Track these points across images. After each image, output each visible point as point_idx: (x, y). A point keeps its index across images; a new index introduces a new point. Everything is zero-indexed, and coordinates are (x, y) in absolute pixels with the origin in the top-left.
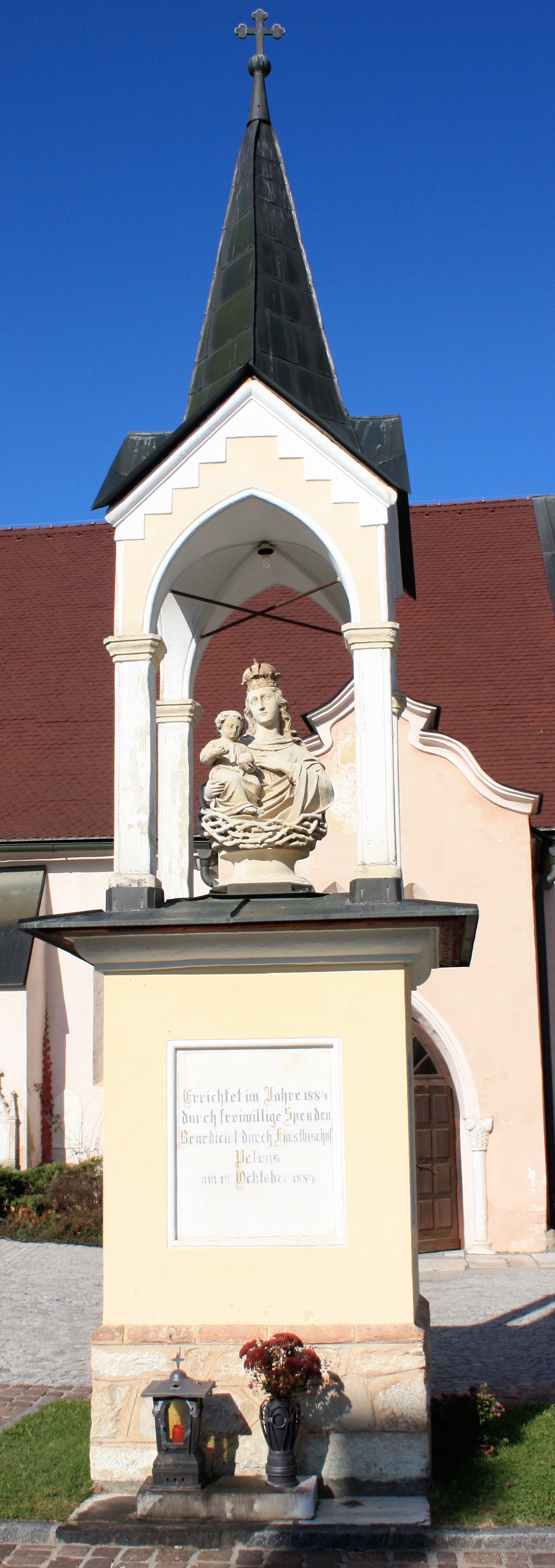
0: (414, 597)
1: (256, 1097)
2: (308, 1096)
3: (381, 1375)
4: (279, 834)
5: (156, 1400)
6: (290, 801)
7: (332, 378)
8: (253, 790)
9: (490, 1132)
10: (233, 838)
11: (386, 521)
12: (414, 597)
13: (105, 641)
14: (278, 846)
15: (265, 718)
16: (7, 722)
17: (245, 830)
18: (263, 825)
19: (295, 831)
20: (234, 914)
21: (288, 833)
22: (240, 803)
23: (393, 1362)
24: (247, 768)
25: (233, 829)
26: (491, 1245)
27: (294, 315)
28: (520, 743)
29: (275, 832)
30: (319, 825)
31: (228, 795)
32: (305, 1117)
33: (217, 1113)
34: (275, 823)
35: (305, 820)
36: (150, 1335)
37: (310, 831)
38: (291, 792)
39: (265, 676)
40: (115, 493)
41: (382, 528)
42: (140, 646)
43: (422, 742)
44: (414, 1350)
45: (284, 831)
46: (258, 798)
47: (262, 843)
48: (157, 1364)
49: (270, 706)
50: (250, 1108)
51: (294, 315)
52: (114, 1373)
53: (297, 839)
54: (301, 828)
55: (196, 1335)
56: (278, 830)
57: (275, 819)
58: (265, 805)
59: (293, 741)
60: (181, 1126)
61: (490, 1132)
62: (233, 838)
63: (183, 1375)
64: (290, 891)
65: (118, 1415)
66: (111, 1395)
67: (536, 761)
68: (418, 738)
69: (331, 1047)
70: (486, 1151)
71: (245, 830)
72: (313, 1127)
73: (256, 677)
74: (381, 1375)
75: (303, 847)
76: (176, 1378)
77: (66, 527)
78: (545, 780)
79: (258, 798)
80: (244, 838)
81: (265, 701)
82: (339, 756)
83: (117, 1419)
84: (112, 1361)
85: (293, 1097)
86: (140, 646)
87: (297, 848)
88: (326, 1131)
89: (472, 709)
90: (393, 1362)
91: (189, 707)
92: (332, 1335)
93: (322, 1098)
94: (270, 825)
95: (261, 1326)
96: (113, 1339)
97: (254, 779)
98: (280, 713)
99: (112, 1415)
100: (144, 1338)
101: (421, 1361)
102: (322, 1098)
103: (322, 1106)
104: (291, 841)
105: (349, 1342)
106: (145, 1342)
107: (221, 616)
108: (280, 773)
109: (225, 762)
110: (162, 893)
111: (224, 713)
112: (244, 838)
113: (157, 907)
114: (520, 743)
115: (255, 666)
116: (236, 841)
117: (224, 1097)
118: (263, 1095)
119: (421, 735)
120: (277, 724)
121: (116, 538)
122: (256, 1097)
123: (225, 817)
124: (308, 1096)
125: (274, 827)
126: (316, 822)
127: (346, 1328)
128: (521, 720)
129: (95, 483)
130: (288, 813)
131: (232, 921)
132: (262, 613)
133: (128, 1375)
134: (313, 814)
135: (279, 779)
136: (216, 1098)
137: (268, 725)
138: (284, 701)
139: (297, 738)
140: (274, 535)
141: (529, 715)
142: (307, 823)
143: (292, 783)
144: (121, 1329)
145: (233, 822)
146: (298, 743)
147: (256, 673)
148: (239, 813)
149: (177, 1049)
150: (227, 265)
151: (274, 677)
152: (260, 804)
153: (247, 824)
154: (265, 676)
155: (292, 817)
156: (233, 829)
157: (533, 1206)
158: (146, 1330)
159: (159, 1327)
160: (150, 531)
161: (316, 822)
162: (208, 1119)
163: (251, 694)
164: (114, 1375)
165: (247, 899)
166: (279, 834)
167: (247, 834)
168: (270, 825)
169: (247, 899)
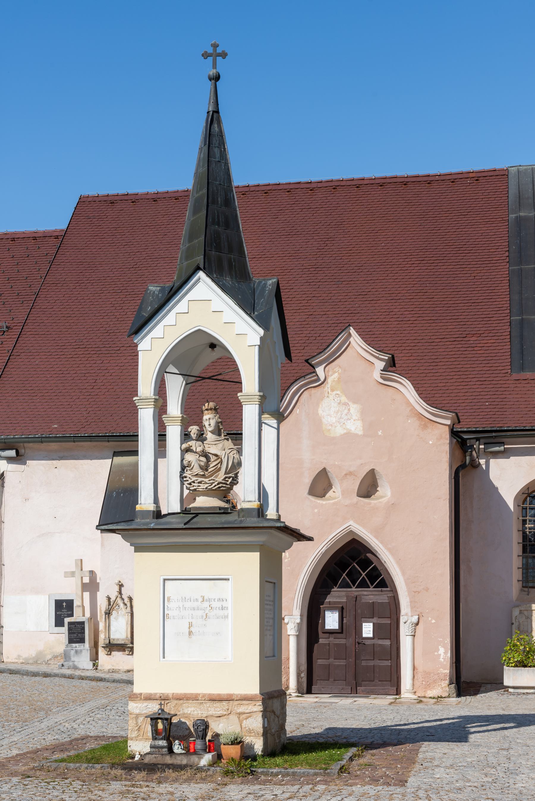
0: (291, 360)
1: (197, 600)
2: (219, 600)
3: (244, 713)
4: (214, 485)
5: (151, 719)
6: (220, 469)
7: (245, 258)
8: (202, 464)
9: (417, 624)
10: (193, 486)
11: (259, 344)
12: (291, 360)
13: (134, 399)
14: (215, 490)
15: (210, 429)
16: (124, 348)
17: (199, 483)
18: (206, 480)
19: (221, 483)
20: (185, 524)
21: (218, 484)
22: (197, 470)
23: (249, 708)
24: (200, 454)
25: (194, 482)
26: (415, 692)
27: (227, 225)
28: (469, 366)
29: (212, 484)
30: (233, 480)
31: (192, 467)
32: (217, 609)
33: (181, 606)
34: (212, 480)
35: (226, 478)
36: (152, 697)
37: (228, 483)
38: (221, 465)
39: (211, 409)
40: (137, 331)
41: (257, 347)
42: (149, 402)
43: (381, 377)
44: (258, 704)
45: (216, 483)
46: (205, 468)
47: (206, 488)
48: (153, 707)
49: (213, 422)
50: (195, 604)
51: (227, 225)
52: (137, 711)
53: (222, 487)
54: (224, 482)
55: (171, 697)
56: (214, 483)
57: (212, 478)
58: (210, 470)
59: (225, 439)
60: (166, 612)
61: (417, 624)
62: (193, 486)
63: (163, 710)
64: (218, 511)
65: (139, 728)
66: (136, 720)
67: (477, 379)
68: (379, 375)
69: (229, 580)
70: (414, 636)
71: (199, 483)
72: (221, 613)
73: (207, 410)
74: (244, 713)
75: (225, 490)
76: (160, 712)
77: (167, 192)
78: (482, 393)
79: (205, 468)
80: (198, 486)
81: (211, 421)
82: (329, 386)
83: (139, 730)
84: (137, 707)
85: (213, 600)
86: (149, 402)
87: (223, 490)
88: (226, 614)
89: (440, 340)
90: (249, 708)
91: (180, 418)
92: (225, 697)
93: (225, 601)
94: (210, 480)
95: (197, 694)
96: (137, 698)
97: (203, 459)
98: (219, 426)
99: (137, 728)
100: (149, 698)
101: (261, 708)
102: (225, 601)
103: (225, 604)
104: (219, 487)
105: (233, 700)
106: (150, 699)
107: (192, 379)
108: (216, 455)
109: (192, 451)
110: (160, 511)
111: (191, 427)
112: (198, 486)
113: (157, 519)
114: (469, 366)
115: (206, 404)
116: (195, 487)
117: (184, 599)
118: (200, 599)
119: (381, 374)
120: (217, 432)
121: (138, 349)
122: (197, 600)
123: (190, 476)
124: (219, 600)
125: (211, 482)
126: (231, 479)
127: (231, 695)
128: (472, 349)
129: (128, 325)
130: (218, 475)
131: (184, 527)
132: (209, 378)
133: (143, 712)
134: (230, 475)
135: (216, 458)
136: (181, 601)
137: (212, 432)
138: (220, 420)
139: (227, 437)
140: (215, 342)
141: (478, 345)
142: (227, 479)
143: (221, 462)
144: (141, 694)
145: (194, 479)
146: (227, 439)
147: (206, 408)
148: (197, 475)
149: (165, 580)
150: (196, 196)
151: (215, 409)
152: (207, 470)
153: (200, 479)
154: (211, 409)
155: (221, 476)
156: (194, 482)
157: (441, 669)
158: (151, 694)
159: (156, 694)
160: (154, 347)
161: (231, 479)
162: (178, 609)
163: (206, 417)
164: (137, 712)
165: (197, 514)
166: (214, 485)
167: (200, 485)
168: (210, 480)
169: (197, 514)
